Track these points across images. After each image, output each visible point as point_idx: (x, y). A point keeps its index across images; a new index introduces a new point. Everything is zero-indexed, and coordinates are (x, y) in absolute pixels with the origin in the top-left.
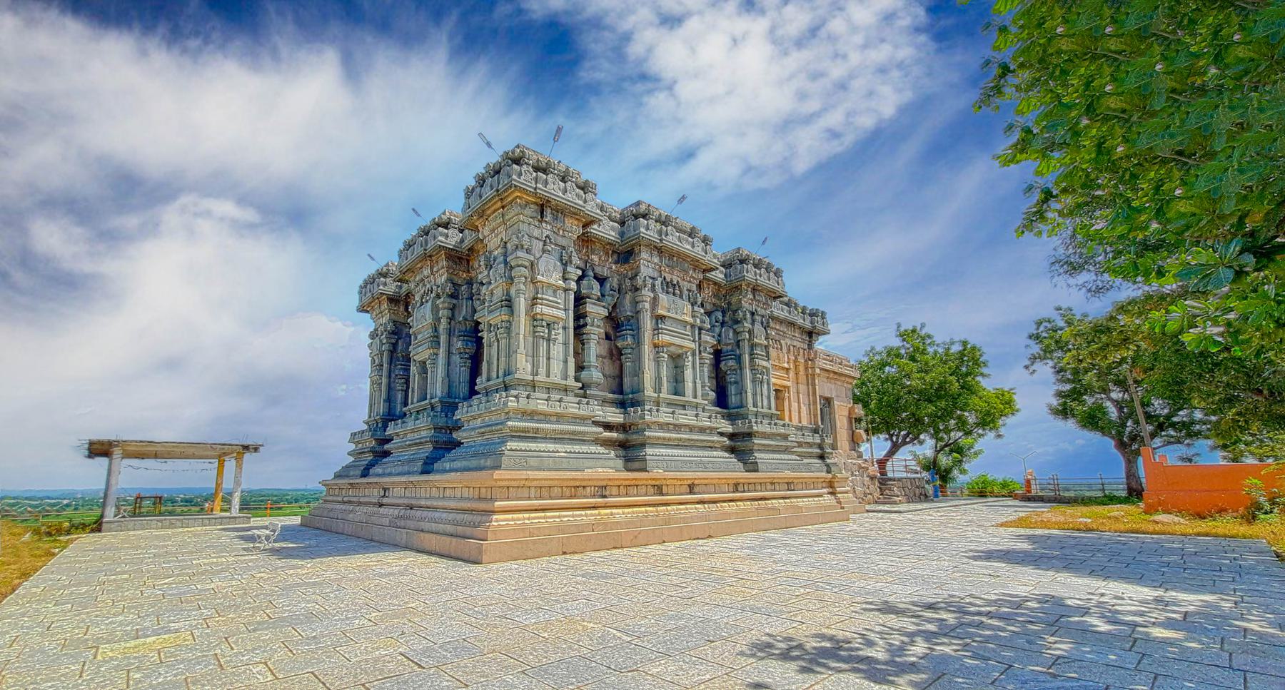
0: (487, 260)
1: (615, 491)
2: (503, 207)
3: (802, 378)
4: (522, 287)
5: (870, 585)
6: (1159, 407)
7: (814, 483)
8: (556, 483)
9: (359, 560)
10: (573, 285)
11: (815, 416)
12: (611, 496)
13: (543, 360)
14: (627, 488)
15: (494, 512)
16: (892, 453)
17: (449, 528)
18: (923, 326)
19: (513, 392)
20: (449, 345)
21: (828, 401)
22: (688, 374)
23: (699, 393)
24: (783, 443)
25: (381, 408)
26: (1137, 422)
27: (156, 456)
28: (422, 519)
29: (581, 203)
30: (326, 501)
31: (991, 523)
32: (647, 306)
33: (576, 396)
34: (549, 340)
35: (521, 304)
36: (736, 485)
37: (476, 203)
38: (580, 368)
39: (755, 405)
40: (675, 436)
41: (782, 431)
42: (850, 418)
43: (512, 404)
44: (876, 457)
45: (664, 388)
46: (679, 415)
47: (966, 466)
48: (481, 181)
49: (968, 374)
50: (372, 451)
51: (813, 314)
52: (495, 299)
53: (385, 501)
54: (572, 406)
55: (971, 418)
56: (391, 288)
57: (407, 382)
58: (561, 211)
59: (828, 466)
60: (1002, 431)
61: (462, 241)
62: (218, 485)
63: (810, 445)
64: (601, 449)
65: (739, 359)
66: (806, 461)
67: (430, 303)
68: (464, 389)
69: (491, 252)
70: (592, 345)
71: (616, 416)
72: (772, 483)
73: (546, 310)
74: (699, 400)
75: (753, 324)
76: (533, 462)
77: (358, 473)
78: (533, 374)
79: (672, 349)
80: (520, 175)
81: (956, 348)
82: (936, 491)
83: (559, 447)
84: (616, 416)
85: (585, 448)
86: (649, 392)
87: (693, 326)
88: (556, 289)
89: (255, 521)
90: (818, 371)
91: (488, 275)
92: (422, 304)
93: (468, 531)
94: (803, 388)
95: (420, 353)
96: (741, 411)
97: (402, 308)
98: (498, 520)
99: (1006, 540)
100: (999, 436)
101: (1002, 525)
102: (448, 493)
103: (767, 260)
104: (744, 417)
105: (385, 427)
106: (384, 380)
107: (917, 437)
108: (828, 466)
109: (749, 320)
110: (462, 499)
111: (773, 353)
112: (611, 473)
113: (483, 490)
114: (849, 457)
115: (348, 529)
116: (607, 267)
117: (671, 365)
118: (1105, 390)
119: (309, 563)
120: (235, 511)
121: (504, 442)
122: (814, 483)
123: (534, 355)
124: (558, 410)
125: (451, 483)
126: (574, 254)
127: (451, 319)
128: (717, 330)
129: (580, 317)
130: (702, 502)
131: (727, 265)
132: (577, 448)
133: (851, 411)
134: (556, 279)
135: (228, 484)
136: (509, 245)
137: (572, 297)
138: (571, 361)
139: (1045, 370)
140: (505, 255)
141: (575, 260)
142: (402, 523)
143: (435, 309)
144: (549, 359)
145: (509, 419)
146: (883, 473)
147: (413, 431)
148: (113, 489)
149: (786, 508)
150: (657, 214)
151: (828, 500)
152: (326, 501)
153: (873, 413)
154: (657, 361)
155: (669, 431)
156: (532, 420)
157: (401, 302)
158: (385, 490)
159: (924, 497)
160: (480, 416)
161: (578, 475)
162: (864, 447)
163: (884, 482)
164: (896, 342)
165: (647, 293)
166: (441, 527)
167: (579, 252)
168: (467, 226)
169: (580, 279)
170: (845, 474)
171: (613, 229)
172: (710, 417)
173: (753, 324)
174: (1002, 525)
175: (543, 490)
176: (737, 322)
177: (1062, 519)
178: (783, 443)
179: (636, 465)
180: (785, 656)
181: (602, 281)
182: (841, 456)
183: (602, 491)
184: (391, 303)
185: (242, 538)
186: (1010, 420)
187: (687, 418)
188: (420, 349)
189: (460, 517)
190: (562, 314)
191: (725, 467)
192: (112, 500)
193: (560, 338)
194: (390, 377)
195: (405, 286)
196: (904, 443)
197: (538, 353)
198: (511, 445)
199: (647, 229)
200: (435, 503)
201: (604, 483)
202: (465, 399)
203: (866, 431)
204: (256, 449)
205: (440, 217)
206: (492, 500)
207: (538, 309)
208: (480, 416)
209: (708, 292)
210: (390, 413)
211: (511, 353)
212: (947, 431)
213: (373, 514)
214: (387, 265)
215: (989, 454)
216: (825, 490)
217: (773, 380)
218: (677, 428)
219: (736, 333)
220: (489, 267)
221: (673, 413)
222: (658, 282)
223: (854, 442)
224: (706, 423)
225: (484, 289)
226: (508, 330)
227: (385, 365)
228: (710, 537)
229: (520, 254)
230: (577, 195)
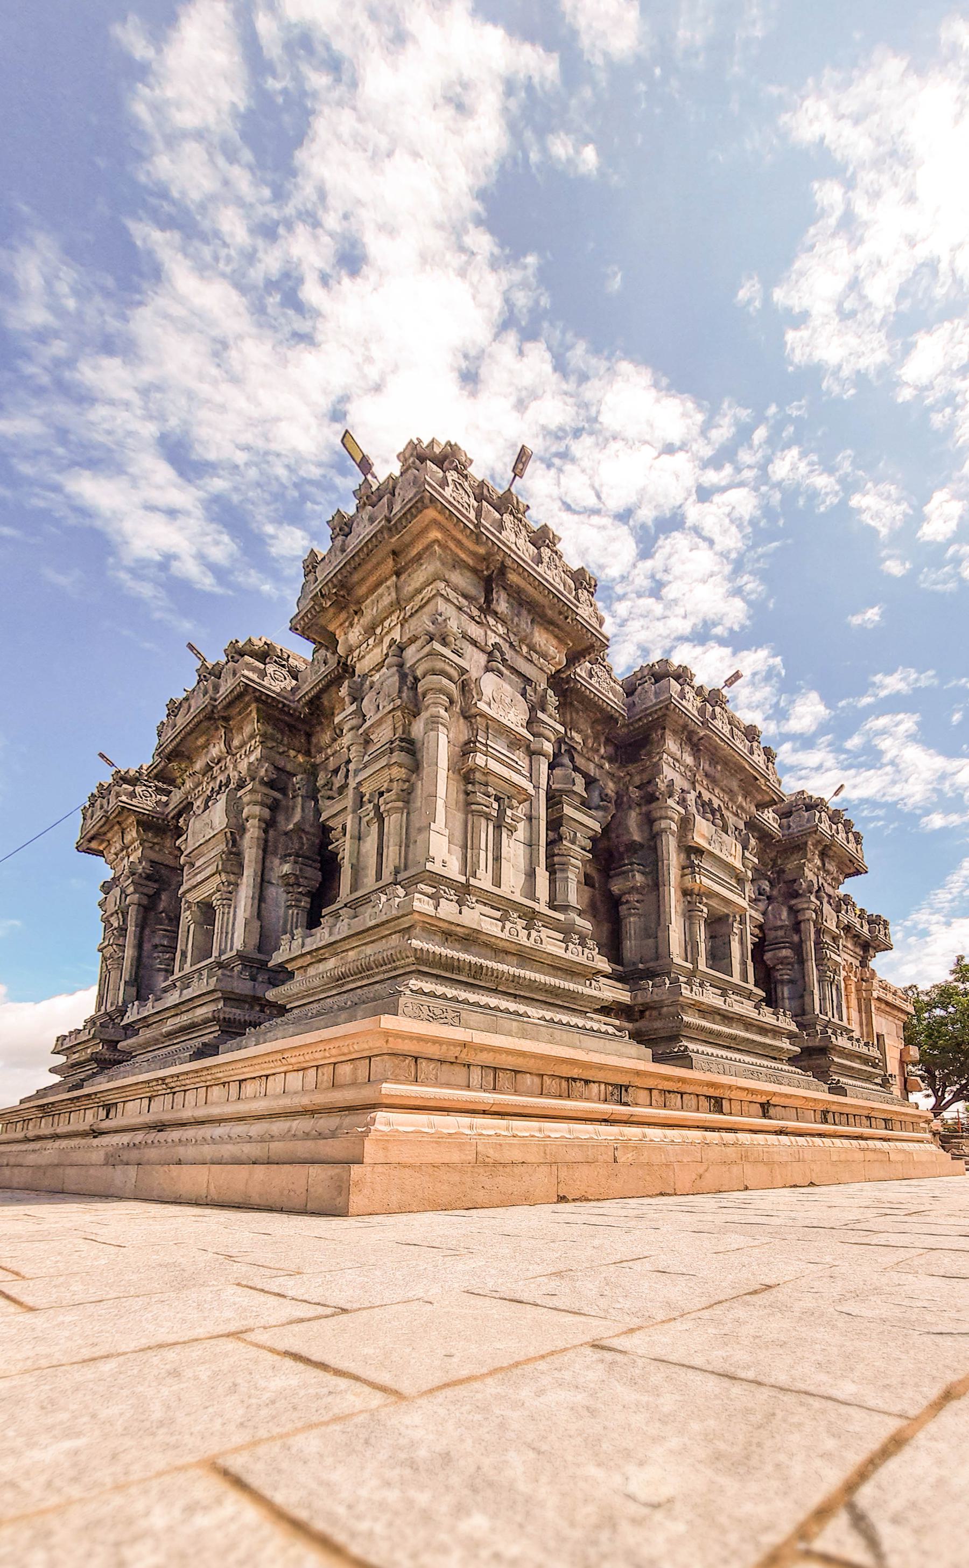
1: (643, 1096)
2: (398, 574)
8: (530, 1064)
15: (374, 1106)
34: (498, 828)
35: (442, 747)
36: (825, 1113)
51: (874, 921)
65: (798, 949)
79: (713, 903)
95: (201, 883)
106: (129, 953)
127: (269, 825)
130: (781, 1132)
143: (234, 808)
154: (689, 915)
157: (163, 828)
176: (796, 895)
183: (620, 1091)
194: (139, 946)
197: (469, 851)
198: (415, 983)
201: (623, 1080)
219: (794, 911)
226: (407, 796)
227: (131, 929)
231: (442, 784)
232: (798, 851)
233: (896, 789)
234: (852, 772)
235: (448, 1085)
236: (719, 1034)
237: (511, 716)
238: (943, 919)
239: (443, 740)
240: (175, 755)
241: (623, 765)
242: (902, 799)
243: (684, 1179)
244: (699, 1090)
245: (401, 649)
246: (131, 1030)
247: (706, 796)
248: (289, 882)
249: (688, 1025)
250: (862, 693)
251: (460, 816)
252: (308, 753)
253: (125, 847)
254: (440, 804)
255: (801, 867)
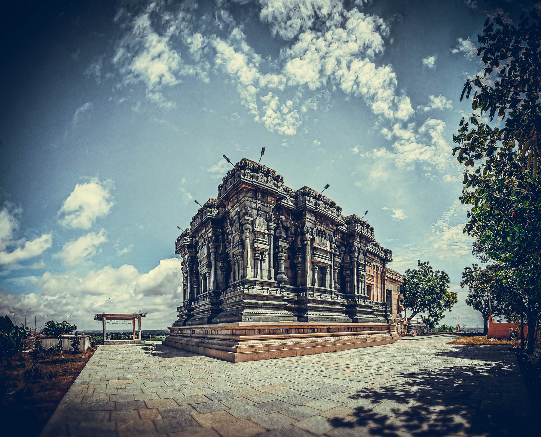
0: (231, 221)
1: (293, 331)
3: (379, 281)
4: (248, 234)
5: (400, 367)
6: (495, 303)
7: (382, 328)
9: (185, 359)
10: (273, 232)
11: (384, 298)
12: (291, 333)
13: (259, 271)
14: (298, 330)
15: (239, 340)
16: (413, 316)
17: (220, 347)
18: (428, 263)
19: (246, 286)
20: (216, 265)
21: (390, 292)
22: (328, 277)
23: (333, 286)
24: (370, 310)
25: (188, 296)
26: (489, 308)
27: (115, 319)
28: (209, 343)
29: (275, 188)
30: (170, 335)
31: (442, 343)
32: (309, 242)
33: (275, 287)
35: (248, 243)
37: (224, 194)
38: (277, 273)
39: (358, 293)
40: (321, 306)
41: (369, 304)
42: (398, 300)
43: (246, 292)
44: (407, 317)
45: (316, 284)
46: (324, 293)
47: (439, 322)
48: (225, 180)
49: (443, 285)
50: (186, 314)
51: (386, 251)
52: (235, 242)
53: (193, 335)
54: (273, 292)
55: (442, 303)
56: (188, 241)
57: (198, 284)
58: (266, 193)
59: (388, 320)
60: (452, 309)
61: (218, 213)
62: (134, 329)
63: (381, 311)
64: (287, 312)
65: (352, 270)
66: (379, 318)
67: (206, 247)
68: (222, 286)
69: (232, 218)
70: (282, 262)
71: (293, 296)
72: (364, 328)
73: (260, 246)
74: (333, 289)
75: (359, 254)
76: (256, 318)
77: (181, 323)
78: (254, 277)
79: (321, 264)
80: (244, 175)
81: (440, 274)
82: (427, 331)
83: (268, 311)
84: (293, 296)
85: (279, 312)
86: (309, 285)
87: (331, 253)
88: (264, 235)
89: (147, 343)
90: (386, 278)
91: (232, 230)
92: (202, 247)
93: (229, 348)
94: (379, 285)
95: (204, 270)
96: (352, 295)
97: (194, 250)
98: (241, 344)
99: (449, 348)
100: (450, 311)
101: (448, 344)
102: (219, 332)
103: (367, 223)
104: (353, 297)
105: (191, 304)
106: (189, 284)
107: (423, 309)
108: (388, 320)
109: (357, 252)
110: (225, 335)
111: (367, 268)
112: (292, 323)
113: (234, 331)
114: (397, 317)
115: (180, 346)
116: (289, 222)
117: (320, 273)
118: (483, 296)
119: (168, 359)
120: (140, 339)
121: (242, 309)
122: (382, 328)
123: (255, 268)
124: (267, 294)
125: (222, 329)
126: (273, 216)
127: (216, 253)
128: (342, 256)
129: (276, 247)
131: (348, 223)
132: (276, 312)
133: (399, 296)
134: (264, 229)
135: (137, 328)
136: (241, 214)
137: (272, 238)
138: (272, 270)
139: (467, 287)
140: (239, 218)
141: (273, 218)
142: (201, 344)
144: (262, 270)
145: (244, 299)
146: (409, 324)
147: (202, 306)
148: (105, 330)
149: (370, 338)
150: (314, 194)
151: (387, 335)
152: (170, 335)
153: (407, 298)
154: (313, 270)
155: (318, 304)
156: (255, 299)
157: (193, 248)
158: (193, 331)
159: (424, 334)
160: (231, 298)
161: (277, 324)
162: (403, 313)
163: (409, 327)
164: (417, 269)
165: (309, 236)
166: (217, 347)
167: (274, 214)
168: (221, 205)
169: (276, 229)
170: (394, 324)
171: (292, 201)
172: (337, 297)
173: (359, 254)
174: (448, 344)
175: (262, 331)
177: (465, 341)
178: (370, 310)
179: (303, 319)
180: (367, 397)
181: (286, 229)
182: (393, 317)
183: (287, 330)
184: (187, 247)
185: (144, 349)
186: (455, 305)
187: (326, 297)
188: (203, 268)
189: (224, 342)
190: (267, 247)
191: (341, 319)
192: (105, 335)
193: (267, 259)
194: (191, 282)
195: (194, 239)
196: (418, 312)
197: (259, 272)
199: (309, 201)
200: (214, 336)
202: (224, 290)
203: (404, 306)
204: (144, 316)
205: (207, 203)
206: (239, 335)
207: (256, 245)
208: (231, 298)
209: (339, 236)
210: (192, 297)
211: (244, 268)
212: (434, 308)
213: (189, 341)
214: (186, 230)
215: (448, 318)
216: (386, 331)
217: (366, 281)
218: (322, 302)
220: (232, 225)
221: (321, 295)
222: (315, 230)
223: (399, 310)
224: (335, 300)
225: (230, 237)
228: (336, 351)
229: (246, 217)
230: (274, 184)
231: (249, 254)
232: (351, 237)
233: (435, 159)
234: (420, 145)
235: (251, 335)
236: (319, 307)
237: (263, 229)
238: (447, 225)
239: (248, 241)
240: (195, 233)
241: (297, 221)
242: (438, 164)
243: (299, 352)
244: (308, 327)
245: (239, 212)
246: (193, 309)
247: (319, 228)
248: (221, 268)
249: (309, 306)
250: (425, 105)
251: (253, 260)
252: (222, 229)
253: (185, 253)
254: (249, 259)
255: (354, 242)
